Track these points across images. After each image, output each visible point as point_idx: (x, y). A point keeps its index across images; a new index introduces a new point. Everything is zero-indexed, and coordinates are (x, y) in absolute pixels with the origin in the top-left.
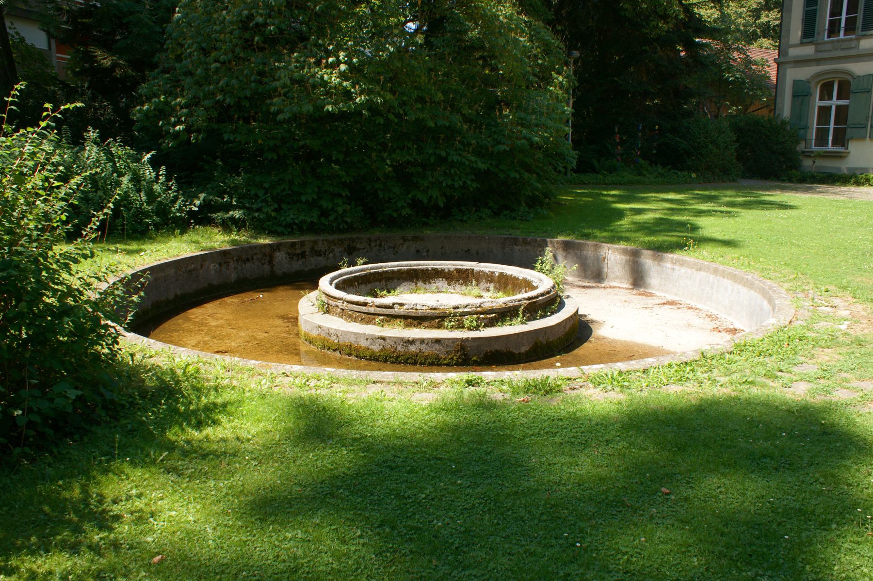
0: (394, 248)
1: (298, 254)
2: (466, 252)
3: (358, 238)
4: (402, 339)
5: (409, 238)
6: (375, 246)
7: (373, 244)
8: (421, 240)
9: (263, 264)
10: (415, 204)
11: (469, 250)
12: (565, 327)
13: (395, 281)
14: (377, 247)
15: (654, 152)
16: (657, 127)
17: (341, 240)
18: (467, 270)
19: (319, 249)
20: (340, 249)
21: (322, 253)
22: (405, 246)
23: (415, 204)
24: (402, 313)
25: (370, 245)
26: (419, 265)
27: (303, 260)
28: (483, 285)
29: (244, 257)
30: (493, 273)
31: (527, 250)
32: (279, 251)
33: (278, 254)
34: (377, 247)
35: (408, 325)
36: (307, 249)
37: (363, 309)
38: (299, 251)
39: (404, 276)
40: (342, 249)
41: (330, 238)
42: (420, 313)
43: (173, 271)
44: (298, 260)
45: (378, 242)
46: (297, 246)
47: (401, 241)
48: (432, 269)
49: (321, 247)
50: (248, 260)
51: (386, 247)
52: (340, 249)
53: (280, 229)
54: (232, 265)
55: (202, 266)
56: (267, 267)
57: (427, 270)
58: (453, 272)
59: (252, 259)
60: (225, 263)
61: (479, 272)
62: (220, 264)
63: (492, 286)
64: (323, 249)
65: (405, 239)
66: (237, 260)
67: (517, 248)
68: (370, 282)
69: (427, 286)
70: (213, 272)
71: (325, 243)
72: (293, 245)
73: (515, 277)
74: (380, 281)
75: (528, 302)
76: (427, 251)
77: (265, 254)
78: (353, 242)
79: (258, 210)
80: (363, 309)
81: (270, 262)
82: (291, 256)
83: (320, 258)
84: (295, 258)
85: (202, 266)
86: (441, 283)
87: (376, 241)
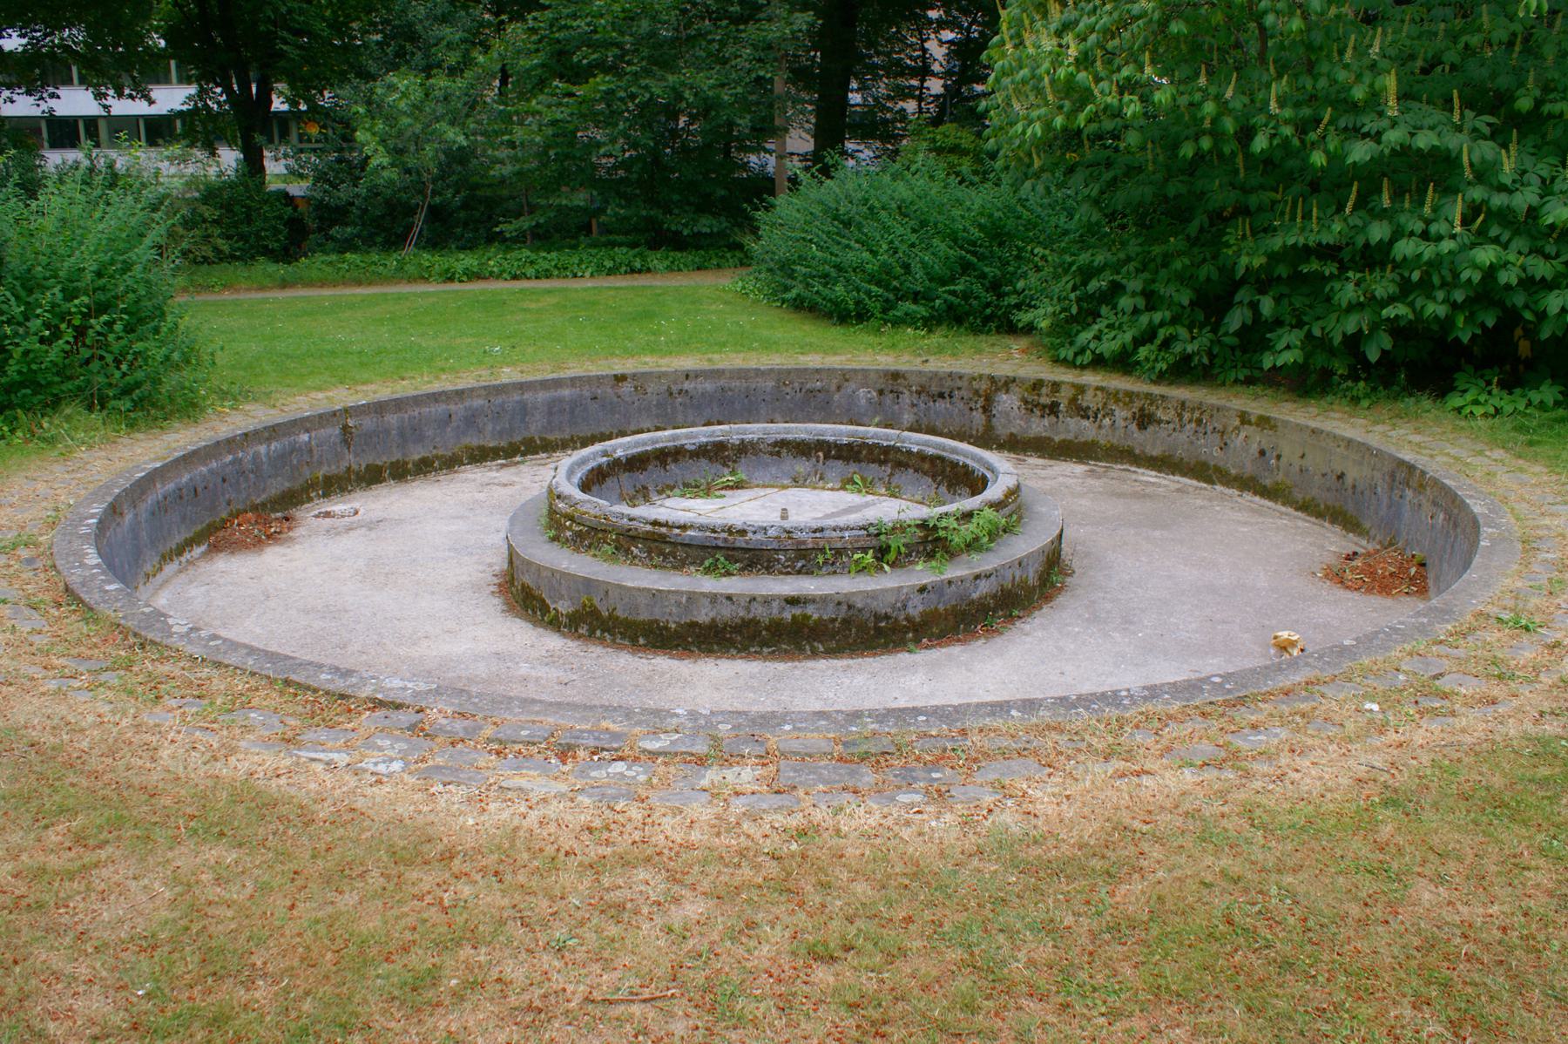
1: (1044, 407)
3: (1163, 396)
5: (1253, 419)
6: (1190, 421)
7: (1187, 416)
9: (971, 409)
19: (1085, 405)
20: (1125, 414)
25: (1180, 416)
29: (934, 389)
32: (1007, 392)
33: (1005, 397)
36: (1064, 397)
38: (1045, 400)
39: (926, 466)
40: (1129, 415)
44: (1043, 416)
45: (1197, 415)
46: (1044, 390)
47: (1237, 422)
50: (941, 396)
54: (906, 398)
55: (839, 388)
56: (978, 417)
59: (951, 397)
60: (892, 391)
62: (881, 392)
64: (1093, 406)
66: (919, 393)
68: (858, 460)
70: (863, 402)
71: (1099, 393)
74: (881, 463)
75: (649, 528)
76: (1279, 457)
77: (976, 392)
78: (1151, 404)
81: (986, 409)
82: (1030, 406)
83: (1085, 423)
85: (839, 388)
87: (1193, 410)
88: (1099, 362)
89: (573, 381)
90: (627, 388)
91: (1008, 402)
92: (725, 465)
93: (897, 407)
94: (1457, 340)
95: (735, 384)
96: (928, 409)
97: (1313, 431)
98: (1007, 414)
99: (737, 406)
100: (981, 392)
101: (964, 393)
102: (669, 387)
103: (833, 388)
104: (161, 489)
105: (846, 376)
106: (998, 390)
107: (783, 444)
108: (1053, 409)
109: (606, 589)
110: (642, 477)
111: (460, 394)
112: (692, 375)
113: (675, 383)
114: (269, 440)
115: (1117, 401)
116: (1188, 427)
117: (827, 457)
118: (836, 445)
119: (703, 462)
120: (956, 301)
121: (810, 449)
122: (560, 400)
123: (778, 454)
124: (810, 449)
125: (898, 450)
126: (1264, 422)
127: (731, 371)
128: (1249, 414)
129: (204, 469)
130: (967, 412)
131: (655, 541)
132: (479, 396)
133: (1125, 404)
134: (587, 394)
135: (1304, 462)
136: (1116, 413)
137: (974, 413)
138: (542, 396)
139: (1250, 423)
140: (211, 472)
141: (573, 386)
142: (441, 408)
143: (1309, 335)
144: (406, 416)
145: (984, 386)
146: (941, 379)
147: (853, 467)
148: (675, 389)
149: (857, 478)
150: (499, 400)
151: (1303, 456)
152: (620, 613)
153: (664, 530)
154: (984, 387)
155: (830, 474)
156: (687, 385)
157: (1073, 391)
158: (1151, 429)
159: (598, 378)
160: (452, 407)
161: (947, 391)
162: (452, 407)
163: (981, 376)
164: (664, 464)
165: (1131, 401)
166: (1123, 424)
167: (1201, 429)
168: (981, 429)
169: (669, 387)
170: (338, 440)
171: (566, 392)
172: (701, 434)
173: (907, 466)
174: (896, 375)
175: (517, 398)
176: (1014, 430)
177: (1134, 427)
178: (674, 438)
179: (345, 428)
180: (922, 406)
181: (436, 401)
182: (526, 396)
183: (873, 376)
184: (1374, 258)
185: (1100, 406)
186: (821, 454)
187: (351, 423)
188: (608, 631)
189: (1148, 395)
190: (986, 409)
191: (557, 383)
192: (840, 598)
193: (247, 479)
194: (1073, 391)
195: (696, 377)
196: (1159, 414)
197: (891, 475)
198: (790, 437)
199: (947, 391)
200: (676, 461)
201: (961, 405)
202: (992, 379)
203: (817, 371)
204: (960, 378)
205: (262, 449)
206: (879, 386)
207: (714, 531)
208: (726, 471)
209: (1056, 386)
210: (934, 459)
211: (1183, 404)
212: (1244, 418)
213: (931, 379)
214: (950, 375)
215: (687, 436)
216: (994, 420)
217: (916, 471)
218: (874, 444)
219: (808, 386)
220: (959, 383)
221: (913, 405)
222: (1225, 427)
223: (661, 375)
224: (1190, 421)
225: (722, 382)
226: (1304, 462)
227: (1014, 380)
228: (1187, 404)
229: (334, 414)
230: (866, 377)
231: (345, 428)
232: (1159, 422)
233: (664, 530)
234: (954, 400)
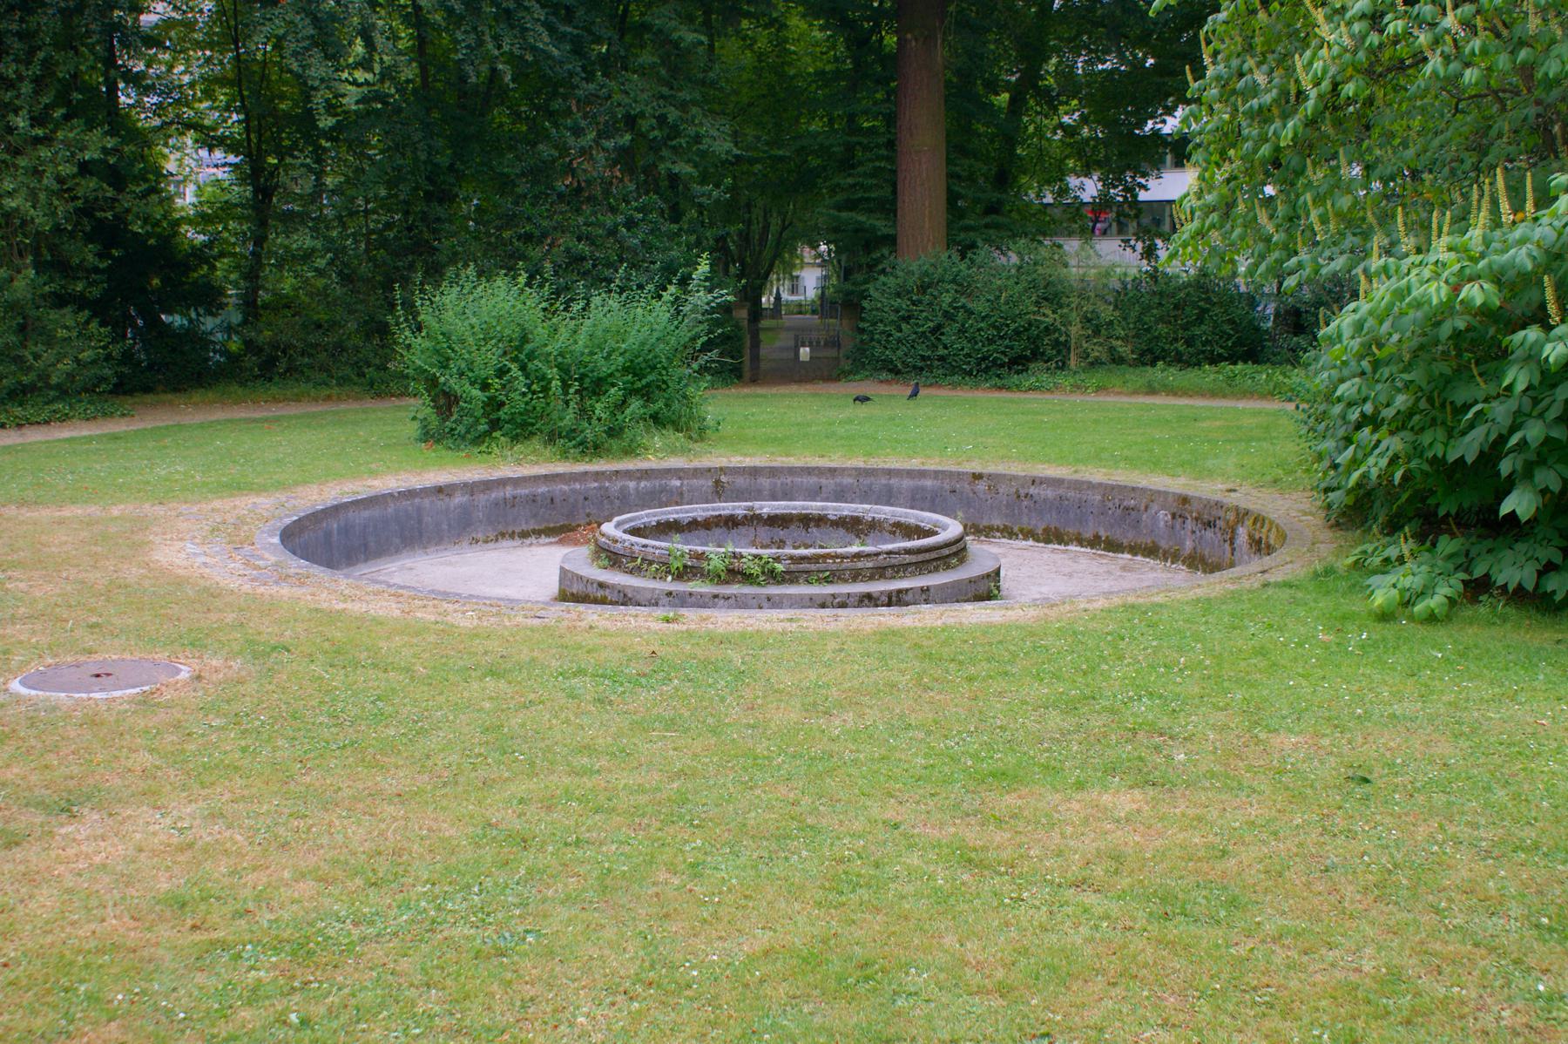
43: (1099, 498)
54: (1189, 524)
55: (1146, 508)
85: (1146, 508)
89: (936, 474)
90: (981, 486)
92: (858, 536)
95: (1071, 494)
99: (1072, 515)
102: (1017, 491)
103: (1143, 508)
104: (509, 491)
107: (898, 525)
110: (781, 533)
111: (832, 471)
112: (1037, 481)
113: (1023, 487)
114: (640, 479)
119: (842, 531)
122: (923, 489)
123: (894, 533)
127: (1070, 482)
129: (565, 488)
132: (850, 475)
134: (947, 487)
138: (907, 483)
140: (574, 491)
141: (936, 478)
142: (813, 480)
144: (779, 482)
148: (1022, 492)
150: (868, 481)
156: (1033, 490)
159: (959, 474)
160: (824, 481)
162: (824, 481)
164: (807, 527)
169: (1017, 491)
170: (710, 491)
171: (929, 483)
172: (847, 509)
174: (1185, 500)
175: (884, 481)
178: (823, 508)
179: (718, 482)
181: (809, 474)
182: (892, 481)
183: (1170, 499)
187: (723, 478)
191: (922, 474)
192: (619, 588)
193: (612, 503)
198: (903, 520)
200: (818, 526)
205: (632, 484)
206: (1172, 511)
208: (857, 541)
215: (835, 509)
221: (1193, 532)
223: (1013, 478)
225: (1061, 492)
229: (709, 470)
230: (1166, 499)
231: (718, 482)
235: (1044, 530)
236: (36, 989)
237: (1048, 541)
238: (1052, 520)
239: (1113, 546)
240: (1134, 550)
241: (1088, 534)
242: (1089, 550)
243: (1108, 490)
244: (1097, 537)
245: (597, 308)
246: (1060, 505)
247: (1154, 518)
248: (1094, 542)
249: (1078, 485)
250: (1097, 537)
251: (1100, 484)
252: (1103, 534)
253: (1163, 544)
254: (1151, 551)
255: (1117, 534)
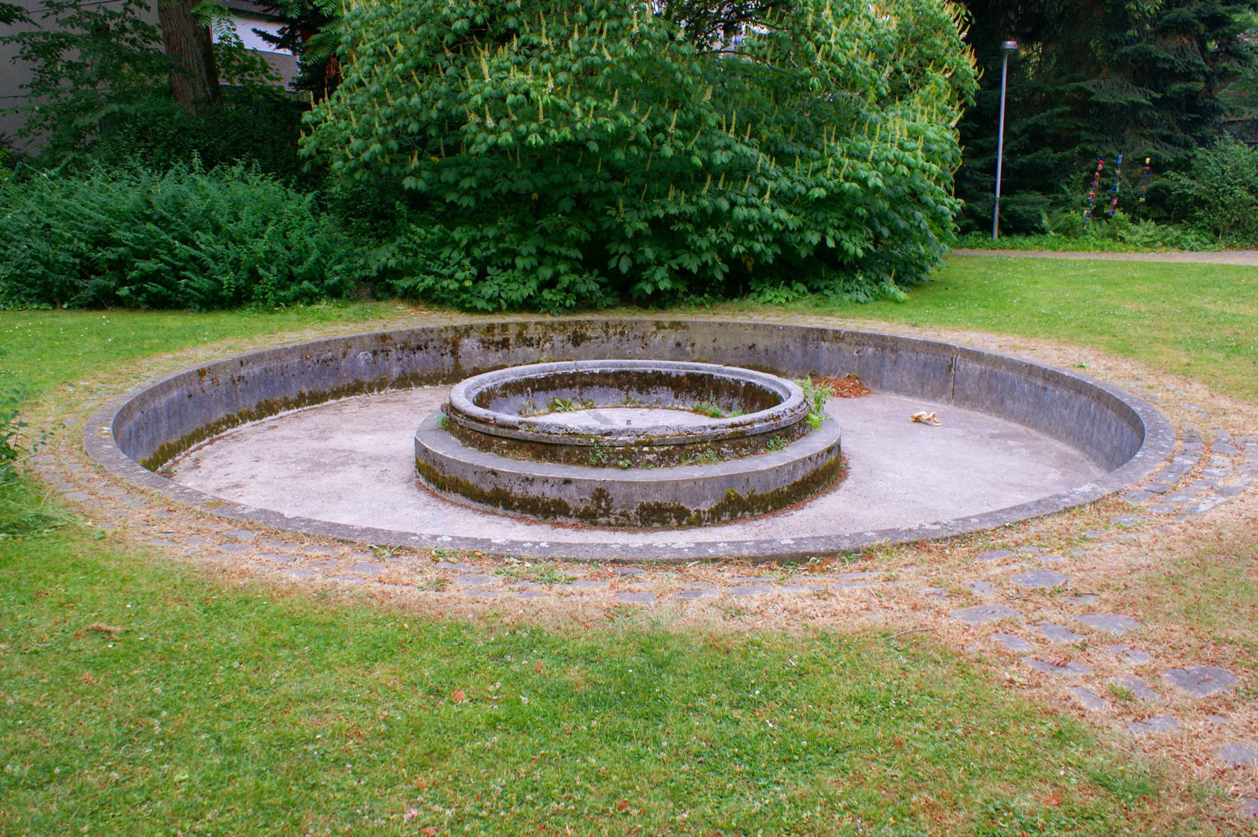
0: (643, 338)
1: (498, 343)
2: (750, 348)
3: (589, 321)
4: (518, 476)
5: (667, 325)
6: (615, 334)
7: (611, 331)
8: (683, 328)
9: (442, 355)
10: (681, 274)
11: (754, 346)
12: (792, 474)
13: (596, 387)
14: (618, 336)
15: (1142, 199)
16: (1148, 160)
17: (563, 324)
18: (703, 375)
19: (528, 337)
20: (561, 338)
21: (534, 342)
22: (660, 336)
23: (681, 274)
24: (530, 438)
25: (606, 332)
26: (635, 365)
27: (505, 350)
28: (724, 400)
29: (413, 344)
30: (738, 382)
31: (840, 349)
32: (468, 336)
33: (466, 341)
34: (618, 336)
35: (537, 457)
36: (512, 334)
37: (482, 427)
38: (498, 338)
39: (611, 381)
40: (565, 338)
41: (548, 319)
42: (553, 439)
43: (297, 360)
44: (497, 350)
45: (619, 329)
46: (496, 331)
47: (654, 329)
48: (654, 372)
49: (532, 333)
50: (419, 348)
51: (631, 336)
52: (561, 338)
53: (480, 304)
54: (394, 354)
55: (344, 355)
56: (448, 360)
57: (645, 373)
58: (683, 378)
59: (426, 348)
60: (383, 351)
61: (719, 381)
62: (375, 353)
63: (736, 401)
64: (536, 337)
65: (659, 325)
66: (402, 349)
67: (825, 345)
68: (554, 388)
69: (644, 397)
70: (363, 363)
71: (539, 327)
72: (490, 328)
73: (764, 390)
74: (571, 387)
75: (731, 430)
76: (693, 345)
77: (446, 341)
78: (581, 328)
79: (451, 277)
80: (482, 427)
81: (453, 353)
82: (486, 344)
83: (531, 349)
84: (493, 348)
85: (344, 355)
86: (664, 394)
87: (616, 327)
88: (513, 307)
91: (469, 345)
93: (387, 363)
94: (766, 262)
96: (410, 361)
97: (720, 324)
98: (469, 353)
99: (277, 384)
100: (449, 340)
101: (436, 343)
103: (340, 356)
105: (348, 343)
106: (461, 336)
107: (506, 386)
108: (505, 344)
109: (746, 478)
115: (554, 330)
116: (613, 338)
117: (533, 391)
118: (539, 381)
120: (919, 244)
121: (522, 386)
123: (505, 395)
124: (522, 386)
125: (582, 374)
126: (675, 325)
128: (662, 322)
130: (439, 357)
131: (737, 438)
133: (560, 331)
135: (716, 344)
136: (554, 338)
137: (445, 357)
139: (664, 327)
143: (671, 269)
145: (450, 335)
146: (417, 335)
147: (551, 394)
149: (557, 401)
151: (715, 341)
152: (758, 493)
153: (740, 429)
154: (451, 336)
155: (539, 404)
156: (243, 372)
157: (519, 328)
158: (583, 344)
161: (423, 344)
163: (446, 328)
165: (565, 328)
166: (561, 345)
167: (625, 338)
168: (451, 369)
173: (592, 384)
174: (384, 337)
176: (475, 365)
177: (570, 345)
180: (405, 358)
183: (367, 340)
184: (716, 219)
185: (541, 336)
186: (529, 389)
188: (748, 509)
189: (577, 323)
190: (453, 353)
194: (519, 328)
195: (248, 362)
196: (589, 333)
197: (581, 394)
199: (423, 344)
201: (434, 353)
202: (455, 329)
203: (327, 343)
204: (432, 331)
206: (372, 349)
207: (766, 421)
209: (504, 327)
210: (617, 375)
211: (607, 324)
212: (659, 325)
213: (409, 336)
214: (423, 330)
215: (613, 365)
216: (460, 360)
217: (601, 386)
218: (563, 374)
219: (323, 357)
220: (431, 336)
221: (399, 359)
222: (644, 334)
224: (615, 334)
225: (265, 365)
226: (716, 344)
227: (472, 327)
228: (610, 323)
230: (362, 342)
232: (590, 339)
233: (740, 429)
234: (429, 350)
235: (257, 407)
236: (898, 476)
237: (261, 417)
238: (261, 395)
239: (317, 398)
240: (337, 394)
241: (293, 396)
242: (296, 410)
243: (305, 351)
244: (302, 396)
245: (135, 322)
246: (266, 379)
247: (354, 361)
248: (300, 401)
249: (277, 354)
250: (302, 396)
251: (295, 348)
252: (305, 391)
253: (367, 379)
254: (356, 388)
255: (320, 387)
